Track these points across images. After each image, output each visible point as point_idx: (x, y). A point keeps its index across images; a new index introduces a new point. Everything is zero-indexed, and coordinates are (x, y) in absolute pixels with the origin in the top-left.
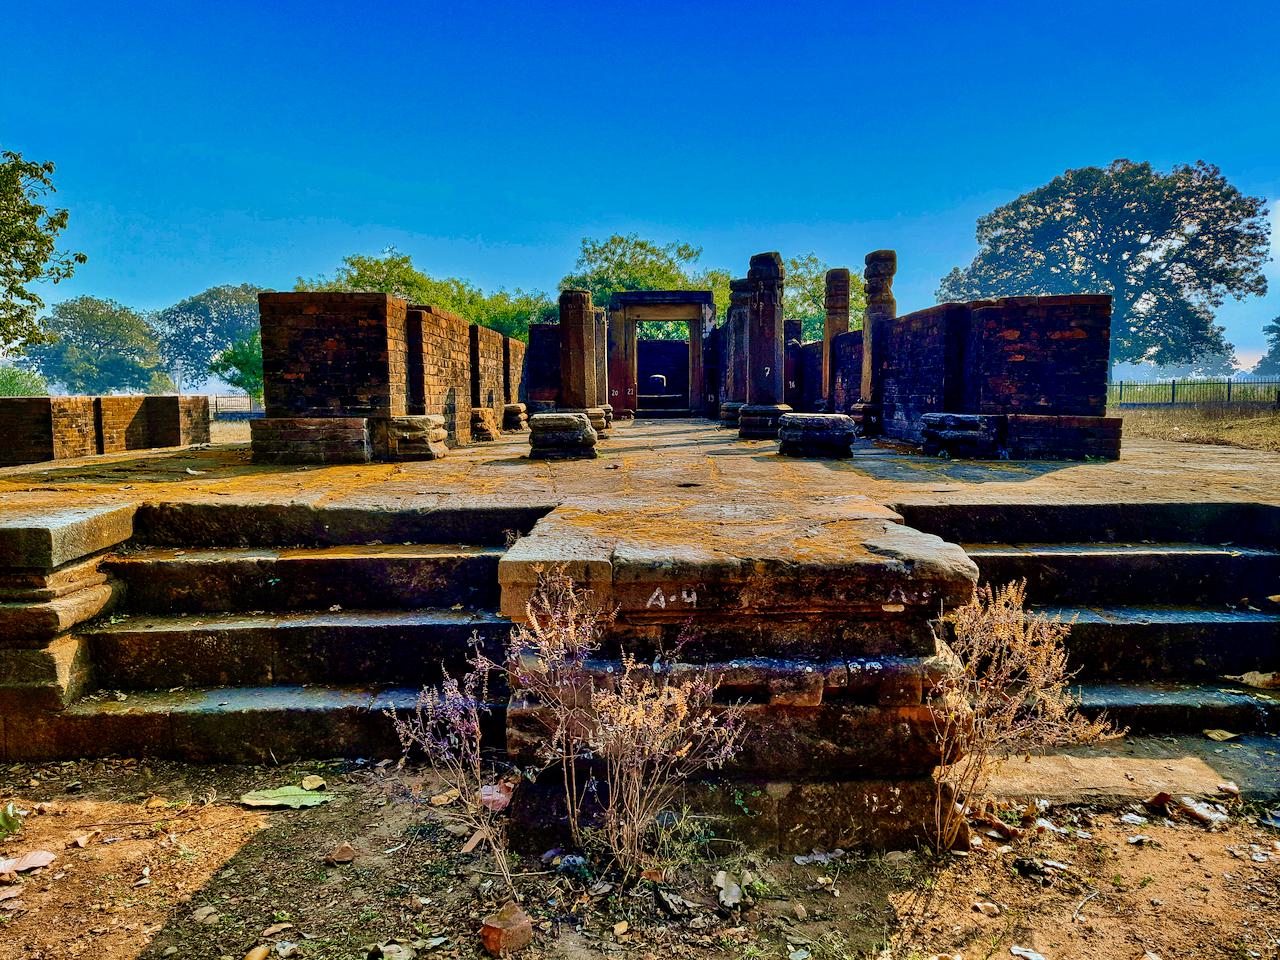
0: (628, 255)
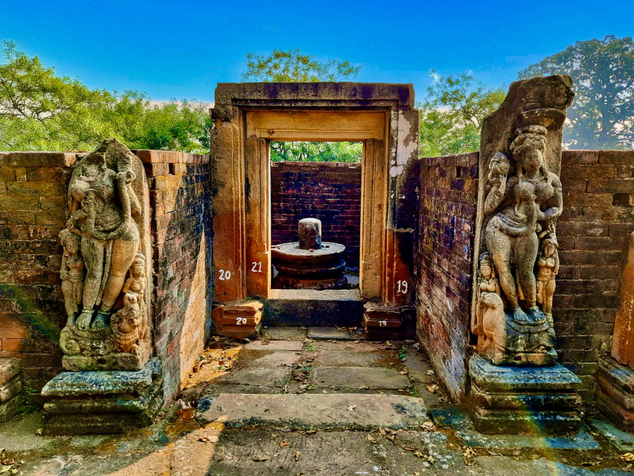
0: (292, 70)
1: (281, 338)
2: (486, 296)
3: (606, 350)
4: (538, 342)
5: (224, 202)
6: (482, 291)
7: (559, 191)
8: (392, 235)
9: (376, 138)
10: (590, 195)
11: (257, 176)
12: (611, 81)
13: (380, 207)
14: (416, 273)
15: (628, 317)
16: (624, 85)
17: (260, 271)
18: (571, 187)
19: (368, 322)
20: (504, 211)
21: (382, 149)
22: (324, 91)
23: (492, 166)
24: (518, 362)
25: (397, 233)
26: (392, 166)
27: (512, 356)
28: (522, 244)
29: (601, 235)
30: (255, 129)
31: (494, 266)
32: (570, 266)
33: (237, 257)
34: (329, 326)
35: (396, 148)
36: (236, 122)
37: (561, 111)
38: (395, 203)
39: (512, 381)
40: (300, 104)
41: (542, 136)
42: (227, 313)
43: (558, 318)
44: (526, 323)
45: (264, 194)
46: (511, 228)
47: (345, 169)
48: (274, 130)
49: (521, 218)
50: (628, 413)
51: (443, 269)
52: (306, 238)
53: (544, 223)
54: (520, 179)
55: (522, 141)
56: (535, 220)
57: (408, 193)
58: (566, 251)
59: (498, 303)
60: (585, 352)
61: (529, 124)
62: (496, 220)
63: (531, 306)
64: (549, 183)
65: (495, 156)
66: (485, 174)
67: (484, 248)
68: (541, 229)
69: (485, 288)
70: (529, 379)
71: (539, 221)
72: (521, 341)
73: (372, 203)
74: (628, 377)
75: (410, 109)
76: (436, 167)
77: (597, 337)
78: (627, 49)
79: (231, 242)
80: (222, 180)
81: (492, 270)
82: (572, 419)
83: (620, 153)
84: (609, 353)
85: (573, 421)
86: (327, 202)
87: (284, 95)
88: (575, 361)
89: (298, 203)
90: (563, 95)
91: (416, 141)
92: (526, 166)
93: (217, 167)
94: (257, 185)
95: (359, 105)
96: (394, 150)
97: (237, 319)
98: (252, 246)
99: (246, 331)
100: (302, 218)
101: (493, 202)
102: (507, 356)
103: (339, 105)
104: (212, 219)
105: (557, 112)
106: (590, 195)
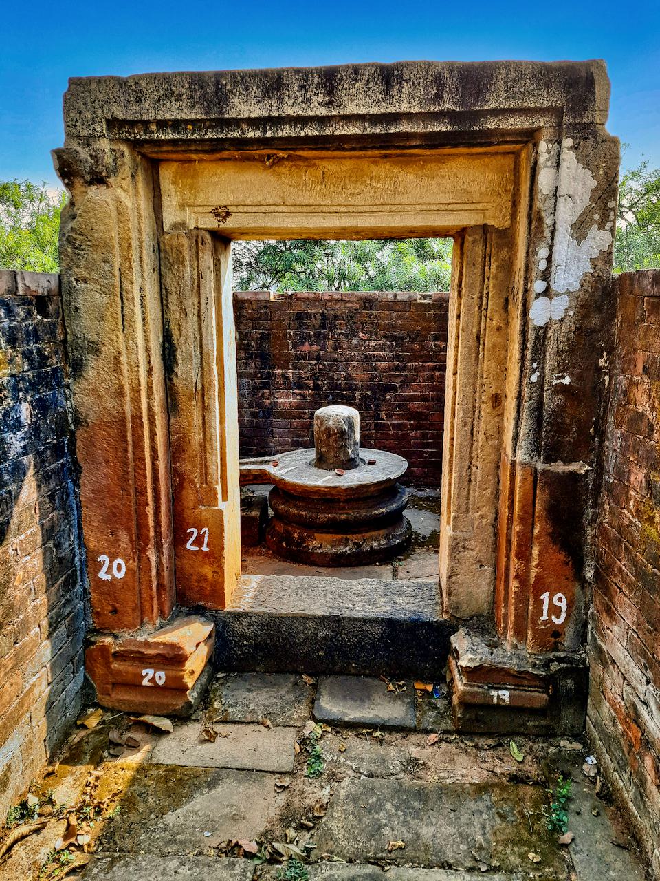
1: (249, 718)
5: (102, 392)
8: (531, 479)
9: (491, 222)
11: (191, 325)
13: (497, 400)
17: (205, 548)
19: (464, 692)
21: (504, 253)
22: (353, 91)
25: (544, 472)
26: (538, 295)
30: (182, 206)
33: (141, 527)
34: (366, 676)
35: (551, 247)
36: (124, 184)
38: (541, 397)
40: (287, 131)
42: (117, 655)
45: (210, 370)
47: (411, 303)
48: (231, 209)
52: (328, 446)
57: (577, 370)
73: (475, 392)
75: (595, 134)
79: (123, 490)
80: (92, 336)
86: (375, 368)
87: (244, 107)
89: (320, 369)
91: (609, 225)
93: (80, 304)
94: (193, 347)
95: (449, 128)
96: (543, 252)
97: (144, 672)
98: (184, 493)
99: (165, 701)
100: (322, 405)
103: (393, 130)
104: (73, 434)
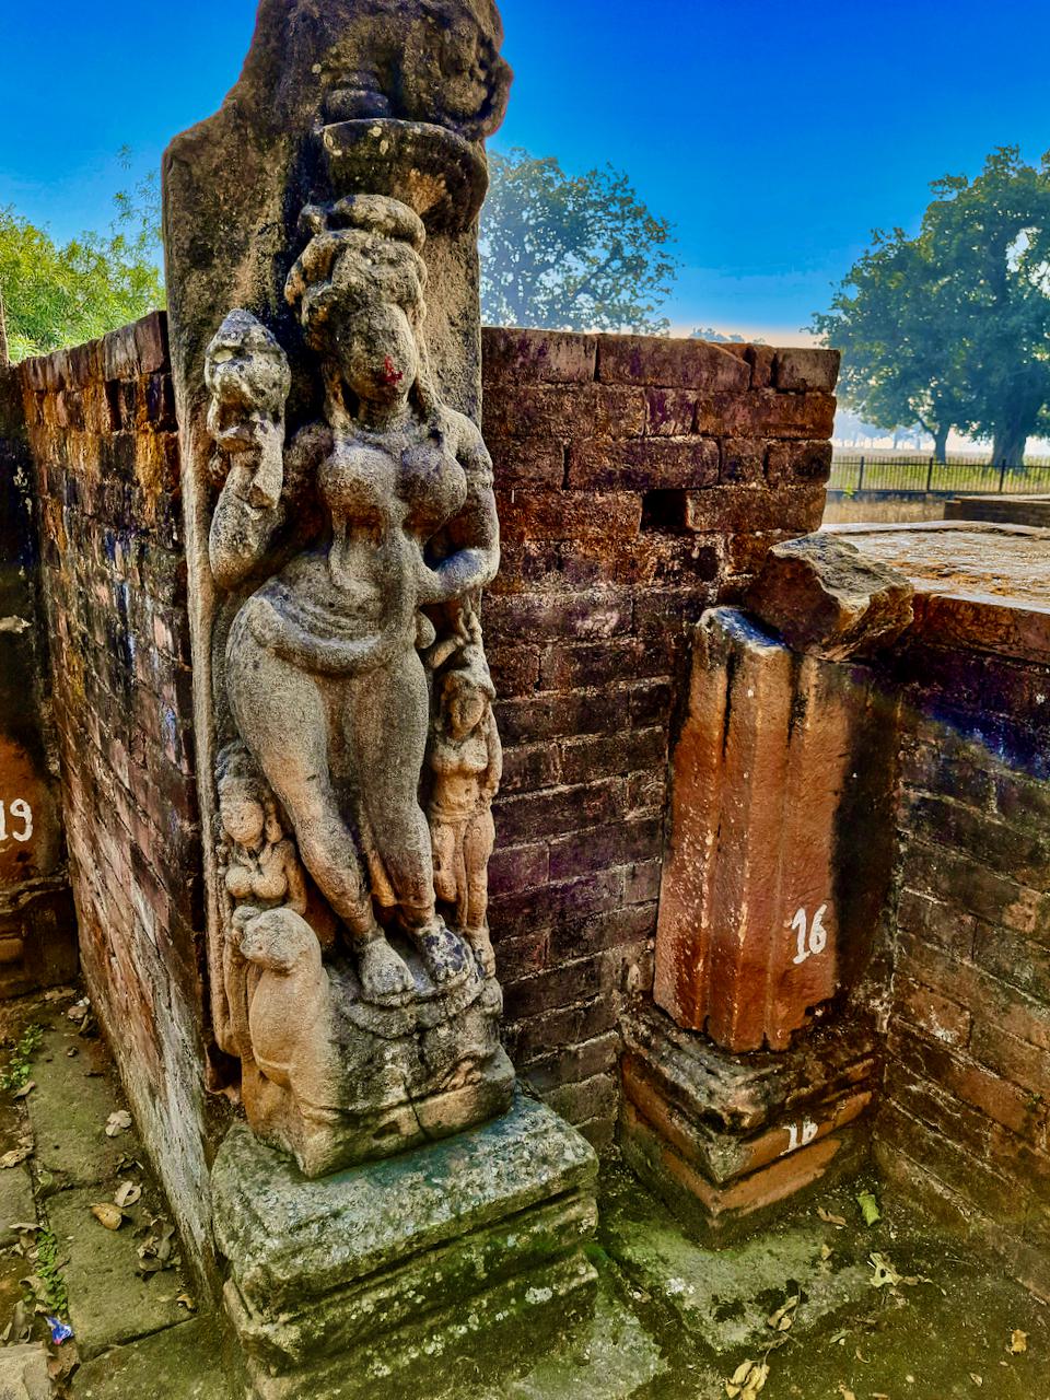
2: (250, 926)
3: (640, 986)
4: (452, 1052)
6: (235, 901)
7: (485, 485)
10: (578, 496)
12: (529, 248)
14: (55, 767)
15: (698, 888)
16: (552, 259)
18: (520, 468)
20: (290, 570)
23: (220, 372)
24: (388, 1142)
27: (367, 1127)
28: (369, 701)
29: (615, 633)
31: (274, 797)
32: (531, 749)
37: (470, 146)
39: (372, 1239)
41: (406, 247)
43: (507, 925)
44: (406, 998)
46: (323, 643)
49: (358, 601)
50: (718, 1194)
51: (117, 777)
53: (443, 614)
54: (339, 435)
55: (328, 265)
56: (410, 605)
58: (518, 699)
59: (299, 948)
60: (587, 1010)
61: (349, 188)
62: (259, 610)
63: (420, 922)
64: (451, 454)
65: (223, 328)
66: (197, 411)
67: (226, 733)
68: (433, 635)
69: (244, 890)
70: (430, 1207)
71: (429, 608)
72: (397, 1065)
74: (714, 1084)
76: (57, 392)
77: (615, 954)
78: (550, 181)
81: (266, 815)
82: (575, 1283)
83: (658, 345)
84: (648, 994)
85: (575, 1289)
88: (560, 1045)
90: (472, 73)
92: (357, 376)
101: (240, 536)
102: (349, 1134)
105: (455, 145)
106: (578, 496)
